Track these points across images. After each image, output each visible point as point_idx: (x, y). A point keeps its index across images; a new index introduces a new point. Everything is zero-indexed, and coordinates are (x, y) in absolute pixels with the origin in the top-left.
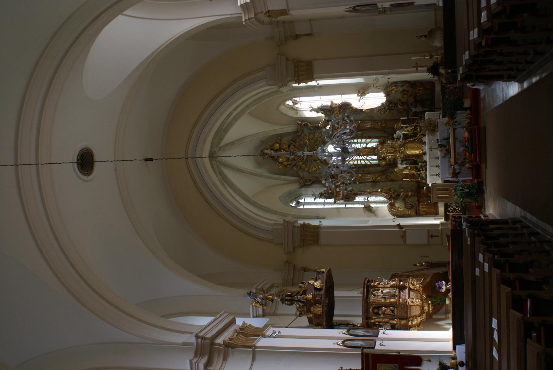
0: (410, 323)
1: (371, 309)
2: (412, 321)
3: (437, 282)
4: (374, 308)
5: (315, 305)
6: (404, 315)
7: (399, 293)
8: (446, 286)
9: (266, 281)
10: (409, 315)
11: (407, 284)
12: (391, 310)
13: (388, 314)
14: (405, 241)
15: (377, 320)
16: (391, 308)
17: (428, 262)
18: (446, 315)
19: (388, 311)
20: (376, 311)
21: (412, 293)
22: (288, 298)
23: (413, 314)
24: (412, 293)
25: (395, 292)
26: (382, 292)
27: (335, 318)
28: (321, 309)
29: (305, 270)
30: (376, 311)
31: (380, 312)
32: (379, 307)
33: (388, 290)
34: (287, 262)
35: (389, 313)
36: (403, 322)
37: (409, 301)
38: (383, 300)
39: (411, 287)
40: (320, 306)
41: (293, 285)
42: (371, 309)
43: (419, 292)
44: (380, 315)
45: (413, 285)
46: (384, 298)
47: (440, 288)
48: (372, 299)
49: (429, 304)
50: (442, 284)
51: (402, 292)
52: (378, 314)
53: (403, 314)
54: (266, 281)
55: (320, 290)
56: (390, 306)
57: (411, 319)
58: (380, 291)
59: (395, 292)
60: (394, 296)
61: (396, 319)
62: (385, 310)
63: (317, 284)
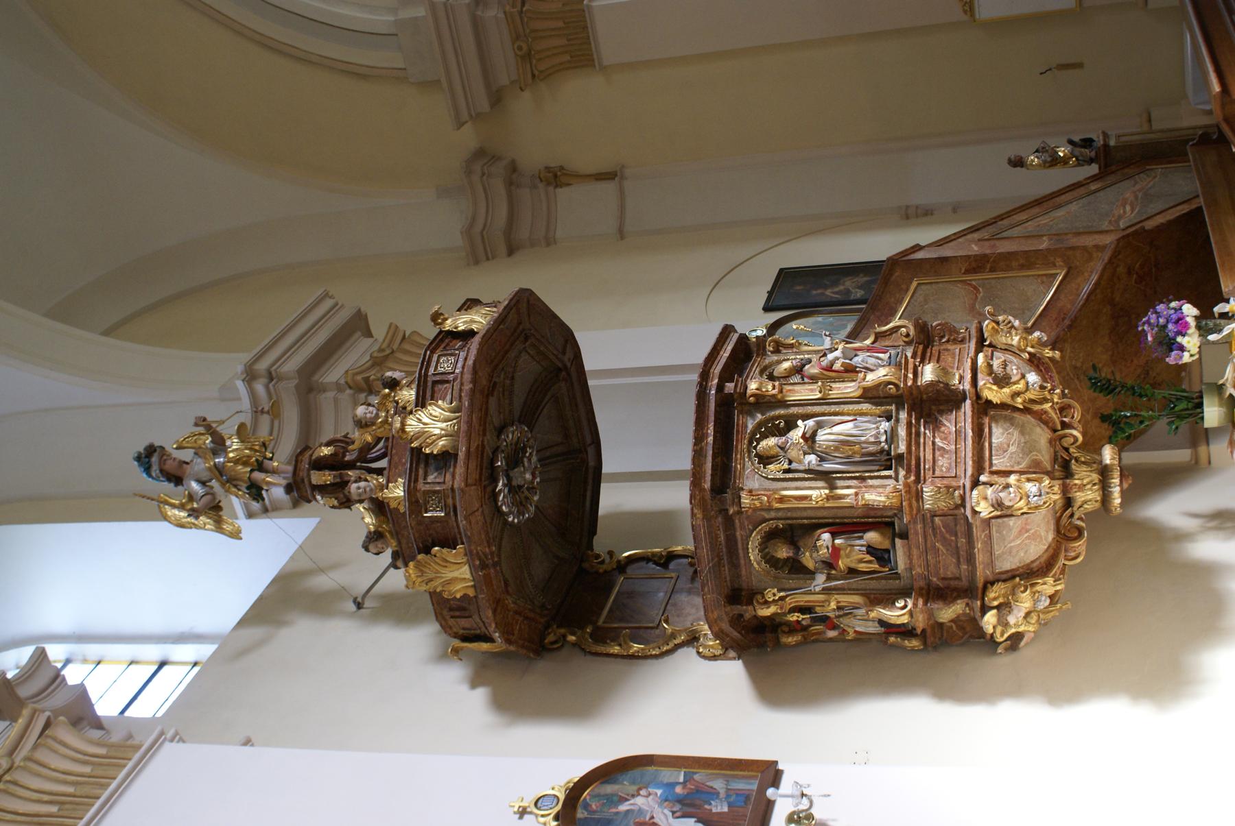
0: (990, 620)
1: (754, 555)
2: (1004, 608)
3: (1150, 304)
4: (772, 536)
5: (427, 551)
6: (951, 571)
7: (914, 437)
8: (1203, 331)
9: (328, 303)
10: (982, 573)
11: (960, 380)
12: (871, 550)
13: (852, 572)
14: (972, 15)
15: (791, 602)
16: (872, 536)
17: (1087, 143)
18: (1194, 444)
19: (855, 552)
20: (783, 552)
21: (999, 435)
22: (318, 478)
23: (1007, 564)
24: (999, 435)
25: (892, 436)
26: (810, 439)
27: (611, 499)
28: (465, 572)
29: (556, 177)
30: (783, 552)
31: (808, 560)
32: (795, 529)
33: (847, 428)
34: (480, 154)
35: (862, 567)
36: (947, 613)
37: (981, 503)
38: (816, 493)
39: (993, 394)
40: (456, 555)
41: (511, 252)
42: (754, 555)
43: (1041, 417)
44: (811, 574)
45: (1002, 381)
46: (827, 477)
47: (1171, 345)
48: (755, 484)
49: (1104, 472)
50: (1180, 320)
51: (936, 425)
52: (796, 568)
53: (949, 567)
54: (328, 303)
55: (445, 459)
56: (864, 527)
57: (995, 595)
58: (796, 435)
59: (892, 436)
60: (885, 460)
61: (905, 593)
62: (836, 551)
63: (433, 423)
